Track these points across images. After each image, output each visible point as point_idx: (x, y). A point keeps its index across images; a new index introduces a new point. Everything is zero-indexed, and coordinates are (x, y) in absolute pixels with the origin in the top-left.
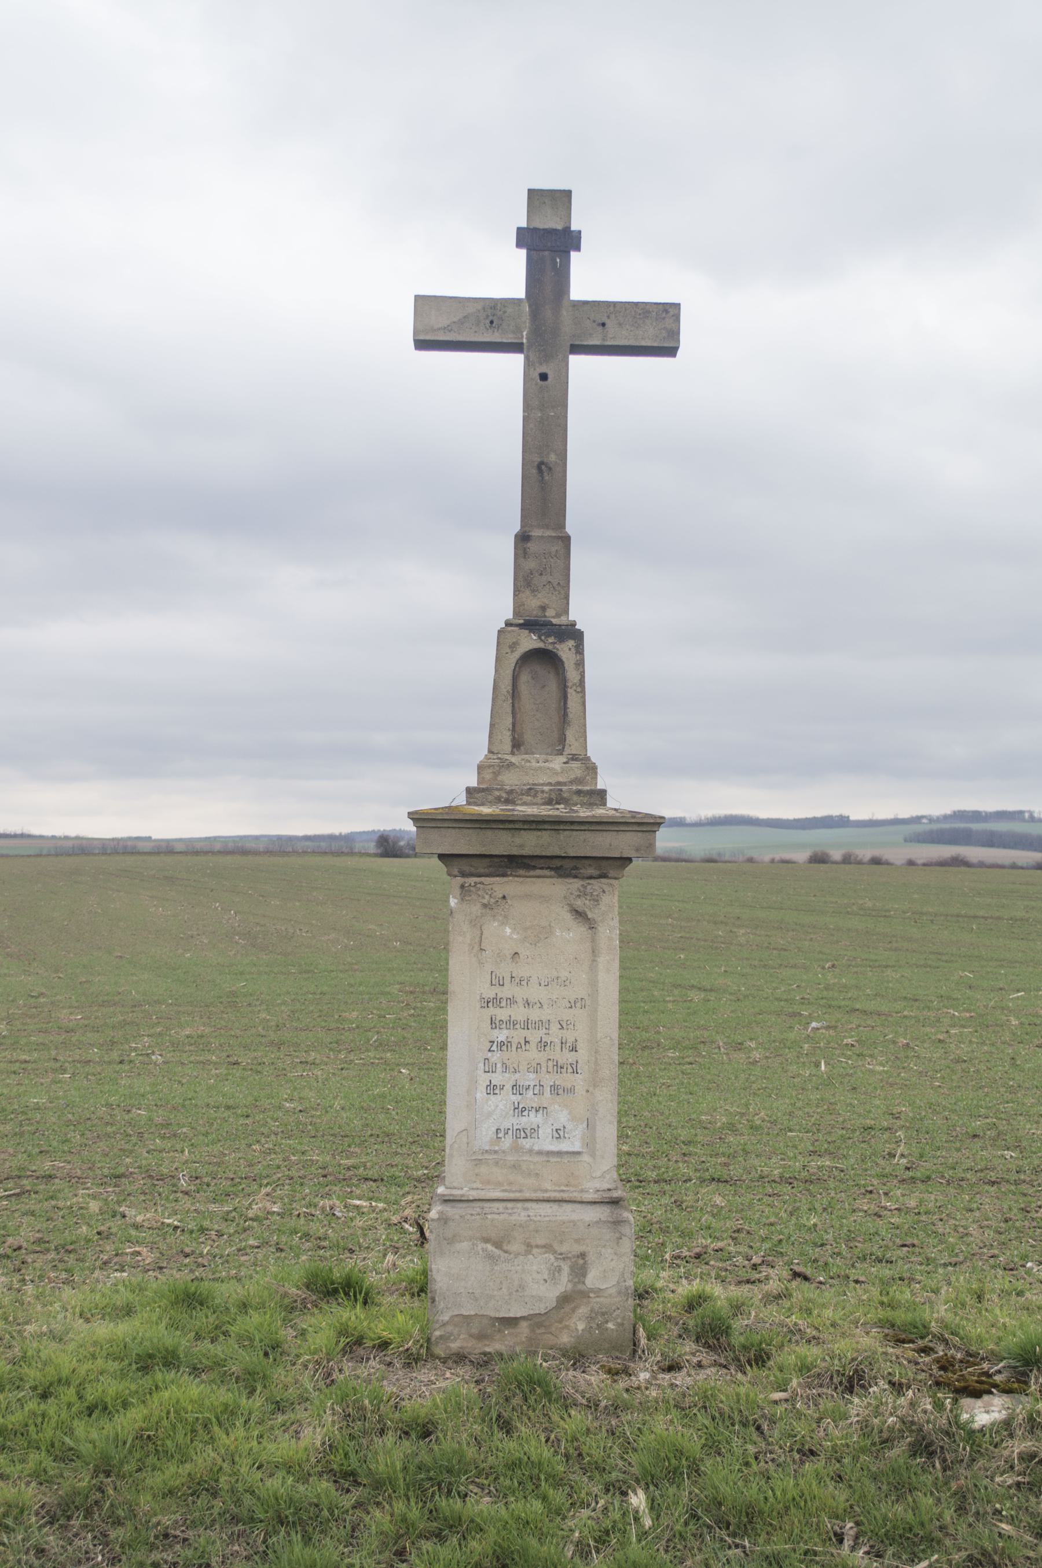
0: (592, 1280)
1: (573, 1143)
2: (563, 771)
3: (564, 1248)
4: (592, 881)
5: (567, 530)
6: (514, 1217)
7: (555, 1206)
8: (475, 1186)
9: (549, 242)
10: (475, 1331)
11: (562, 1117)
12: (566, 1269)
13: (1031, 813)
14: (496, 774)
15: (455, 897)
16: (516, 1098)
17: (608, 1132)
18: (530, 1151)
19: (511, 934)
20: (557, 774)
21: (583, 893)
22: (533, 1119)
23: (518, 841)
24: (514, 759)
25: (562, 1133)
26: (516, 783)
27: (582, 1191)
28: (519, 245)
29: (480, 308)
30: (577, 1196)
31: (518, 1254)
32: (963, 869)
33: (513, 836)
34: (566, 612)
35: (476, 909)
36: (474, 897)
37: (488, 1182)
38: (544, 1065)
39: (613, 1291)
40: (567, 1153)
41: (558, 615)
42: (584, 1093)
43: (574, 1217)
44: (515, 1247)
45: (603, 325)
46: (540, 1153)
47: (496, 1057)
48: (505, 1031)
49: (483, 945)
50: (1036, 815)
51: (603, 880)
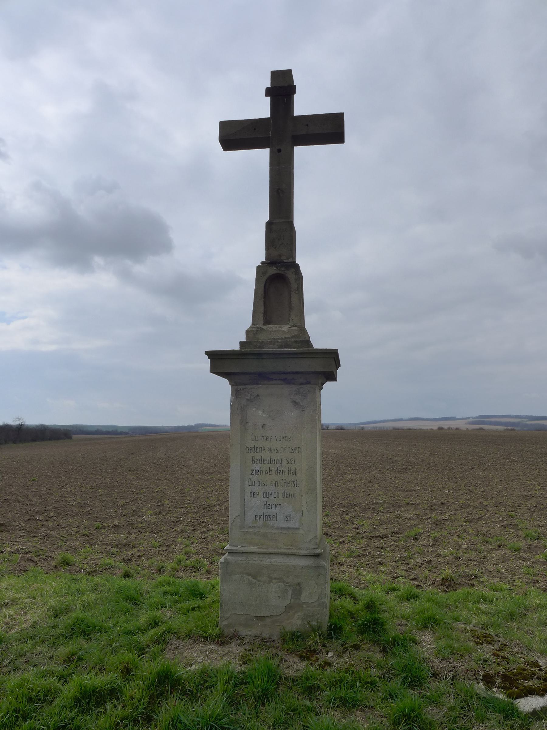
0: (304, 597)
4: (302, 386)
12: (290, 591)
18: (273, 527)
22: (274, 510)
25: (289, 518)
28: (267, 95)
30: (296, 551)
45: (307, 125)
46: (277, 528)
47: (254, 478)
48: (259, 465)
51: (308, 385)
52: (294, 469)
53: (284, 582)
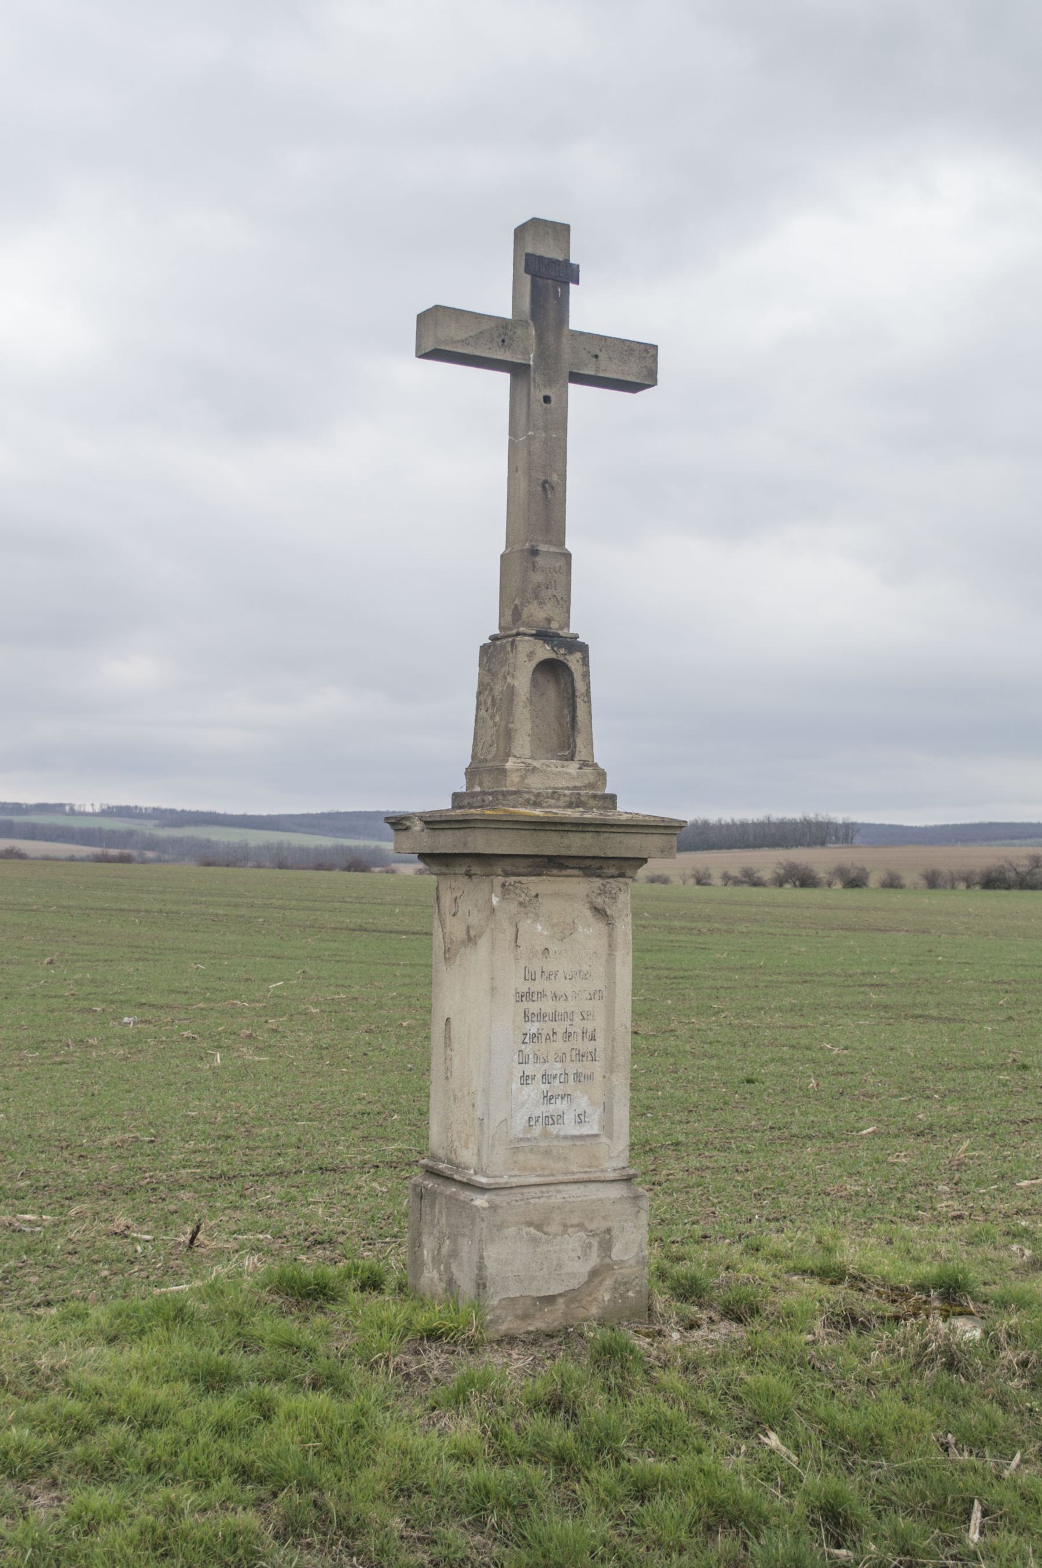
0: (617, 1253)
2: (579, 776)
3: (593, 1226)
4: (611, 880)
5: (566, 546)
6: (552, 1200)
7: (582, 1187)
8: (513, 1173)
9: (546, 268)
10: (519, 1312)
13: (72, 806)
14: (523, 778)
15: (496, 896)
16: (545, 1087)
17: (622, 1113)
18: (557, 1137)
20: (573, 778)
21: (602, 892)
22: (560, 1106)
23: (566, 842)
24: (535, 763)
25: (582, 1117)
26: (540, 786)
27: (602, 1171)
29: (493, 325)
31: (556, 1235)
32: (16, 861)
33: (562, 837)
34: (567, 625)
35: (513, 907)
36: (512, 895)
39: (632, 1262)
40: (588, 1136)
41: (561, 628)
42: (601, 1079)
43: (601, 1195)
44: (554, 1228)
45: (596, 356)
46: (565, 1138)
47: (528, 1049)
48: (536, 1024)
50: (76, 808)
51: (621, 879)
53: (586, 1230)
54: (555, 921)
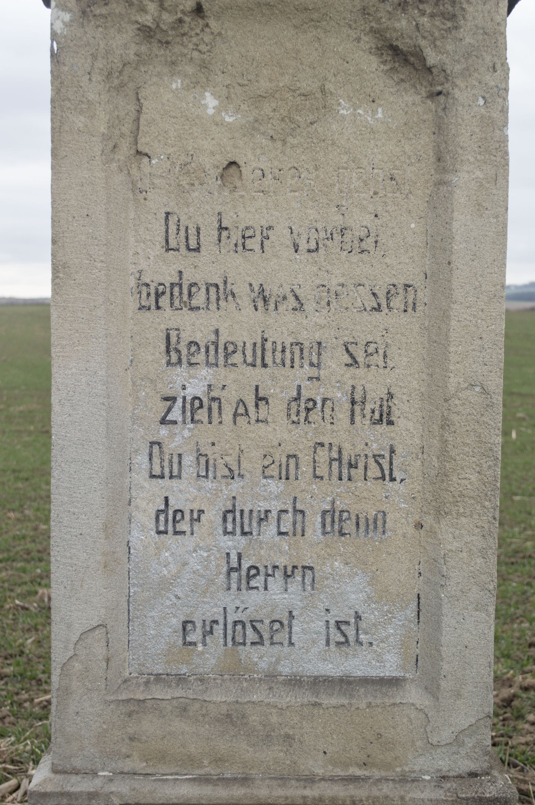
1: (379, 658)
8: (128, 765)
11: (352, 593)
16: (233, 544)
18: (271, 677)
19: (218, 110)
25: (351, 632)
27: (403, 779)
37: (162, 757)
38: (305, 459)
40: (366, 681)
42: (411, 530)
46: (295, 682)
47: (180, 439)
48: (204, 372)
49: (142, 140)
52: (383, 393)
54: (264, 85)
